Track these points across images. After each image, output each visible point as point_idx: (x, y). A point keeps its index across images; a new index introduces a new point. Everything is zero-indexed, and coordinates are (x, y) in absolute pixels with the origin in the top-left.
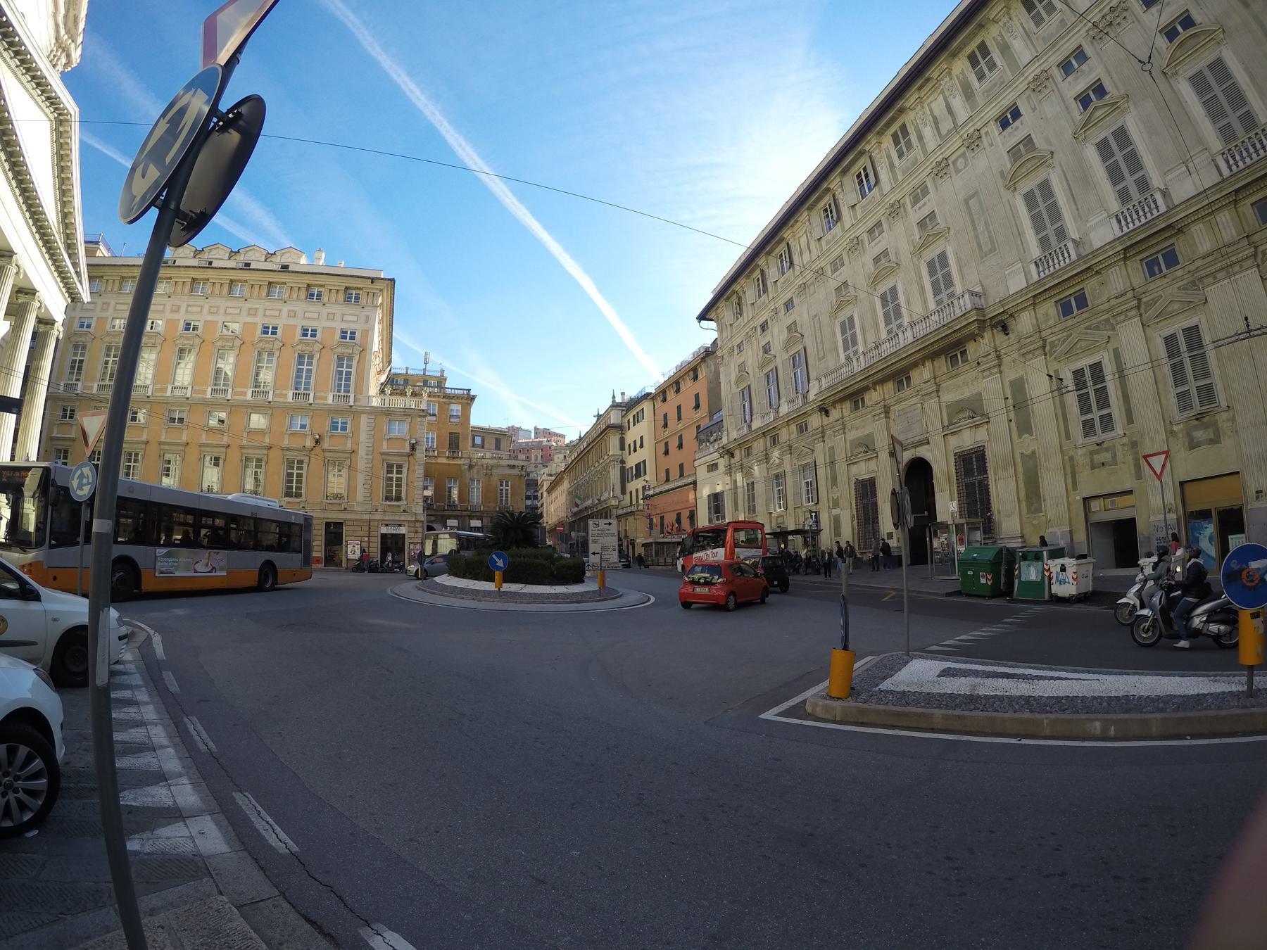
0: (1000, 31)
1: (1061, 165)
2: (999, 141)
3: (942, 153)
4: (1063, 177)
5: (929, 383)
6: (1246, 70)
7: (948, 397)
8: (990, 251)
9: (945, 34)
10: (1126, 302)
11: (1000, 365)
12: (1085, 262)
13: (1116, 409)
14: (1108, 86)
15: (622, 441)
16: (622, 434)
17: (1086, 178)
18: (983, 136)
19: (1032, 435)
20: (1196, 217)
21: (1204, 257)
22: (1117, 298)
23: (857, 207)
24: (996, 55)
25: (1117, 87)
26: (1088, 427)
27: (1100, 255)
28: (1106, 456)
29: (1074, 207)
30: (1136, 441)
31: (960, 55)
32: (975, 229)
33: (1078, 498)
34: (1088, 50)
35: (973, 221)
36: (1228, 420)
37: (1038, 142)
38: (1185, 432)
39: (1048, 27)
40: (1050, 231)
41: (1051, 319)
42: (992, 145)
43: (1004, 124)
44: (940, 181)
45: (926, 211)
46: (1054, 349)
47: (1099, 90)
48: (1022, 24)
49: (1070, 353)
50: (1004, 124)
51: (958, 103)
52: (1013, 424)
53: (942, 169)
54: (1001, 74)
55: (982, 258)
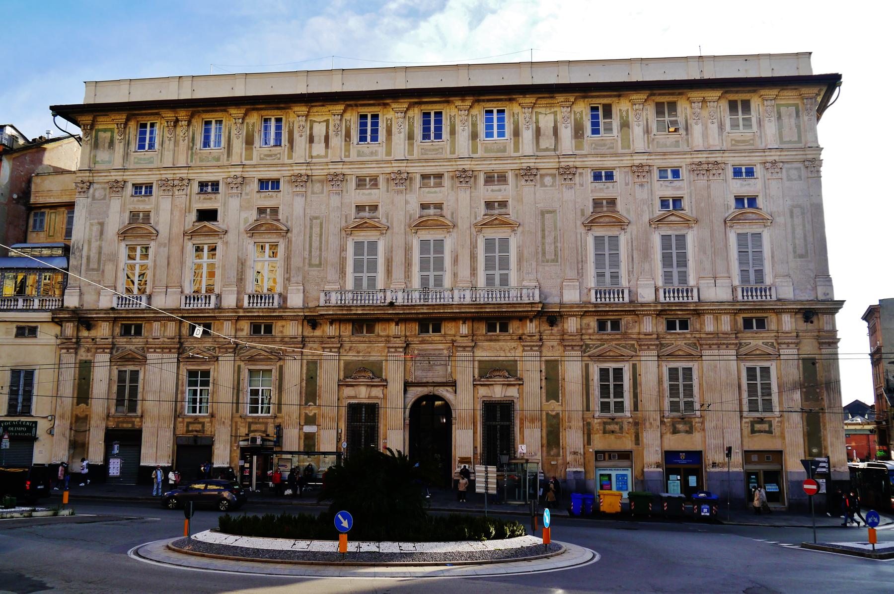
0: (628, 109)
3: (722, 157)
4: (630, 241)
5: (467, 338)
6: (772, 249)
7: (351, 357)
10: (651, 339)
11: (541, 346)
12: (634, 307)
14: (685, 203)
17: (646, 254)
18: (577, 175)
19: (558, 402)
20: (711, 312)
21: (707, 334)
22: (645, 335)
24: (616, 122)
25: (692, 210)
26: (605, 407)
27: (205, 313)
28: (616, 427)
30: (638, 422)
31: (586, 100)
32: (543, 237)
34: (684, 173)
36: (699, 422)
38: (671, 423)
39: (665, 138)
41: (590, 329)
43: (597, 177)
49: (600, 357)
51: (566, 133)
52: (544, 390)
54: (613, 141)
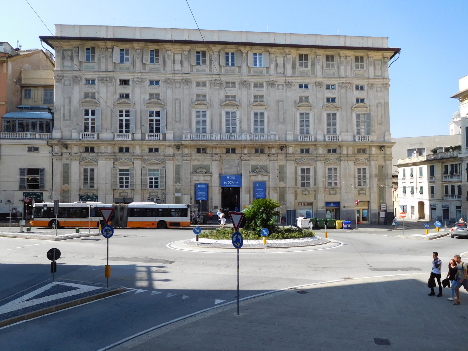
13: (312, 181)
17: (320, 121)
26: (303, 184)
28: (307, 193)
29: (314, 126)
33: (297, 202)
35: (278, 109)
47: (333, 100)
48: (322, 62)
55: (278, 123)
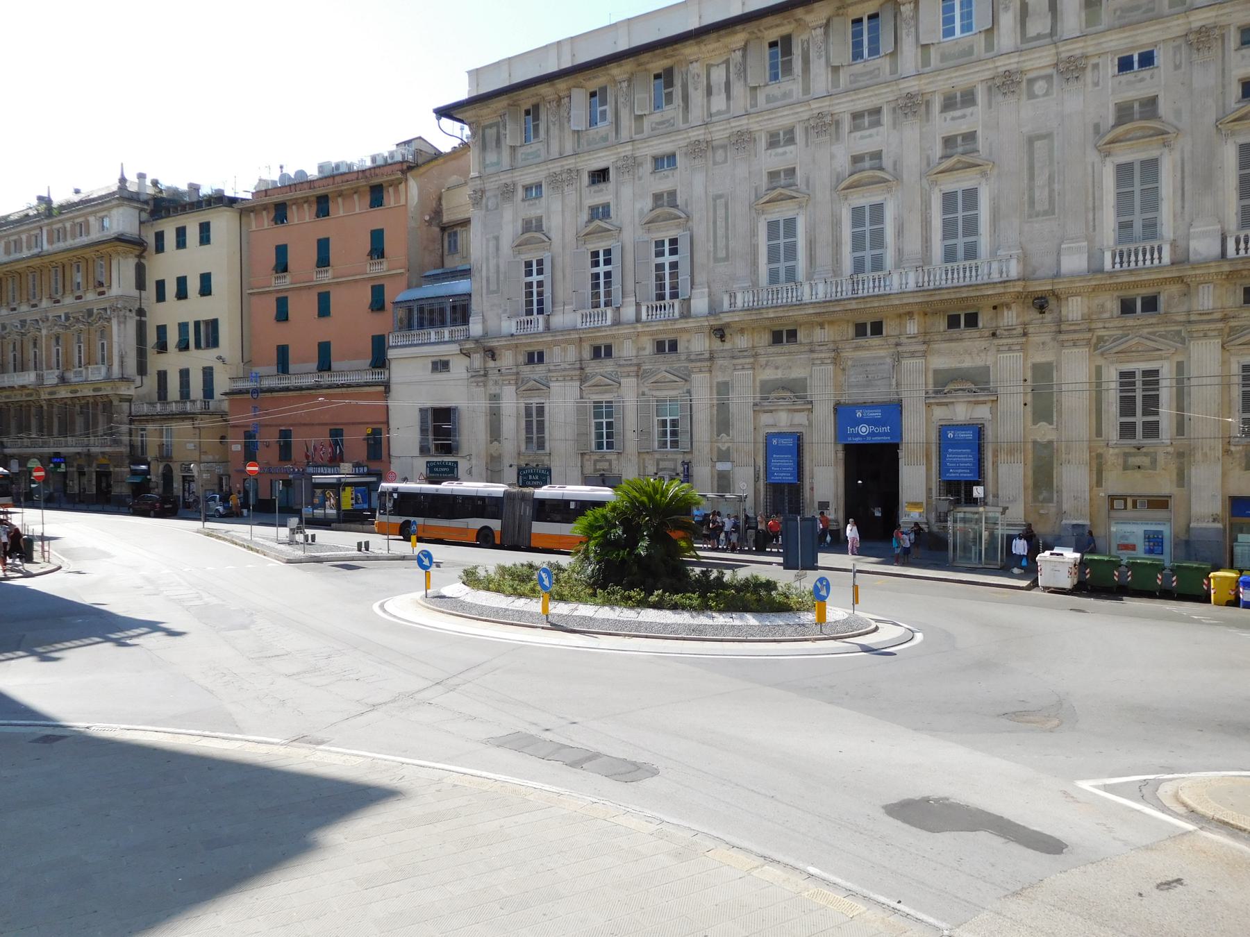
1: (1182, 152)
2: (1110, 84)
4: (1179, 166)
8: (1045, 213)
9: (551, 67)
15: (140, 271)
16: (140, 256)
23: (645, 120)
26: (1127, 430)
29: (1179, 203)
32: (1032, 177)
33: (1103, 495)
35: (1031, 168)
37: (1164, 108)
38: (1243, 454)
40: (1138, 220)
42: (1097, 84)
43: (1125, 64)
44: (1000, 98)
45: (964, 128)
46: (1102, 344)
50: (1125, 64)
52: (1029, 408)
53: (1007, 83)
55: (1030, 216)
